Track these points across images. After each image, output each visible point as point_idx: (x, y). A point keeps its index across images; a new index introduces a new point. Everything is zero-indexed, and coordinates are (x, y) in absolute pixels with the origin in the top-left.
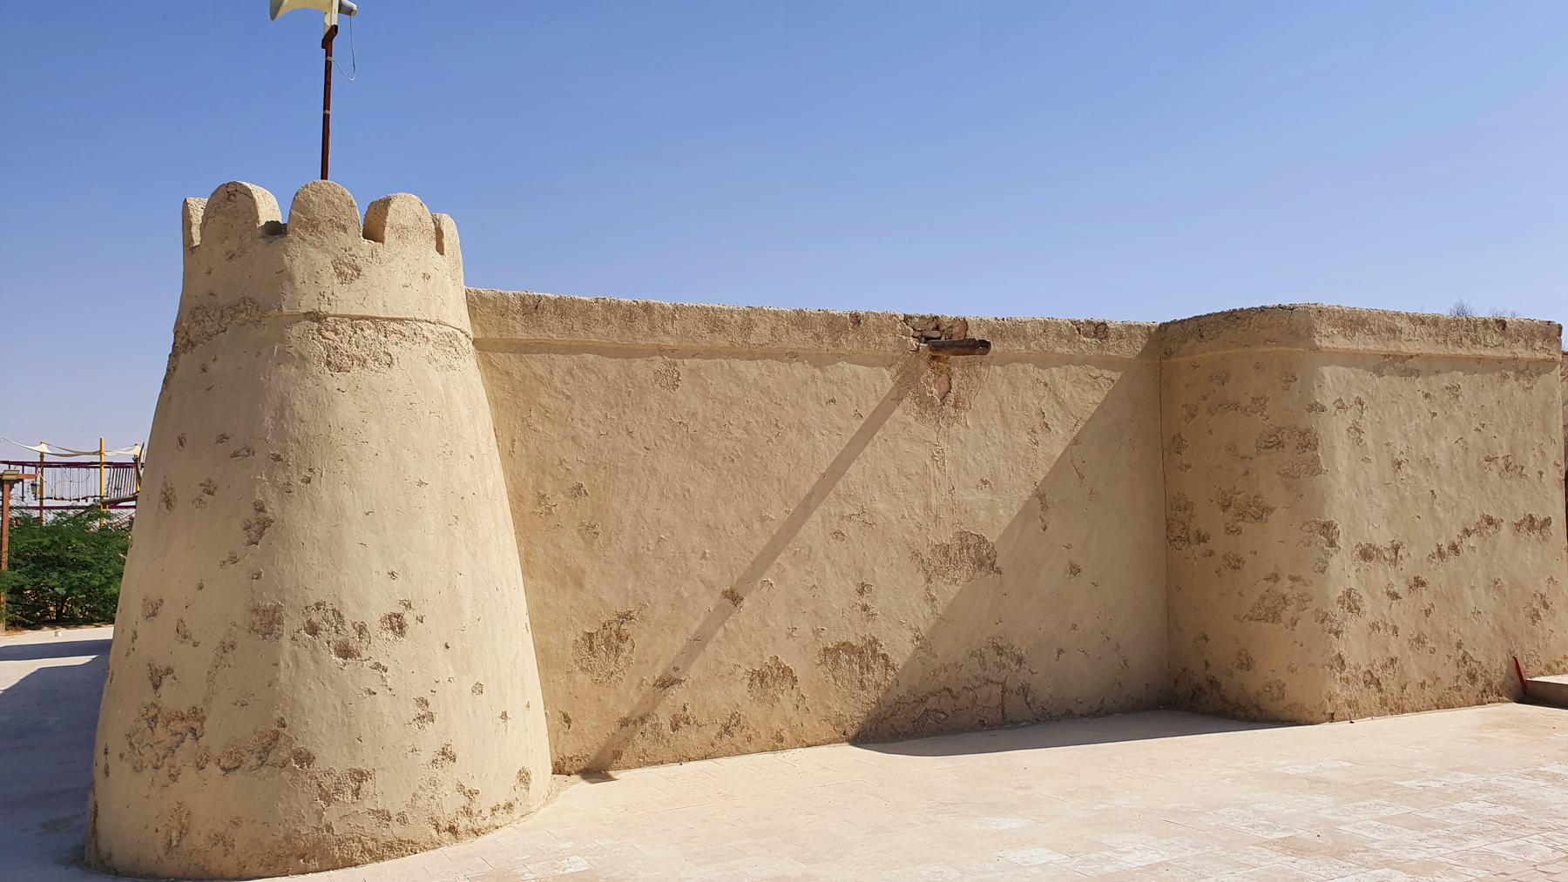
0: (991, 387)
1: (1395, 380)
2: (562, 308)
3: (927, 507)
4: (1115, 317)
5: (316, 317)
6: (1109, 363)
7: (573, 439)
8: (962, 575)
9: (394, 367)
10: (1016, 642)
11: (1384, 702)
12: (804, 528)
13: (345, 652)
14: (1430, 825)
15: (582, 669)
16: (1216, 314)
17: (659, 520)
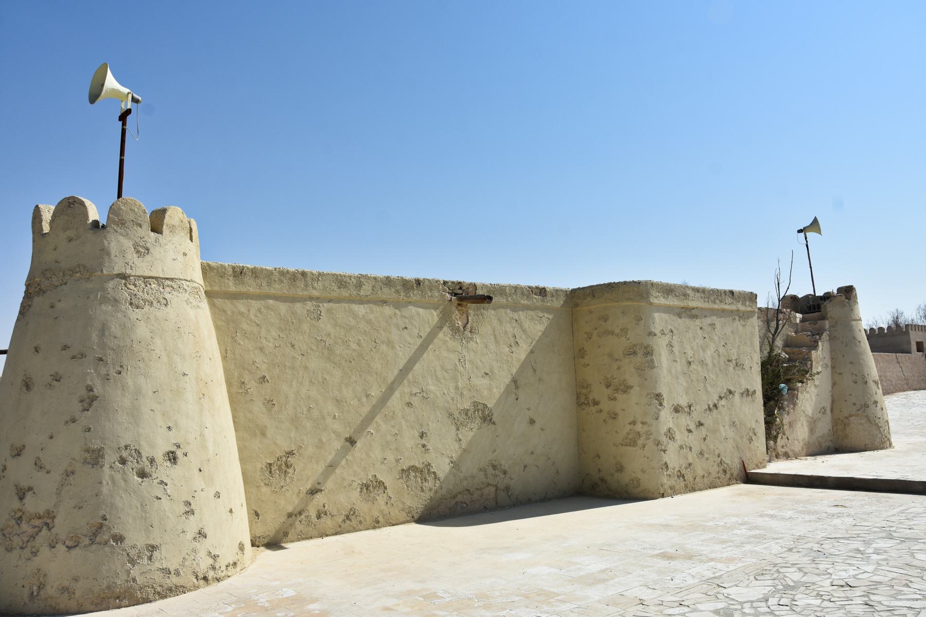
0: (489, 321)
1: (687, 320)
2: (256, 273)
3: (457, 388)
4: (550, 284)
5: (124, 277)
7: (261, 349)
8: (475, 426)
9: (169, 306)
10: (503, 462)
11: (686, 486)
12: (390, 401)
13: (142, 474)
14: (723, 542)
15: (266, 484)
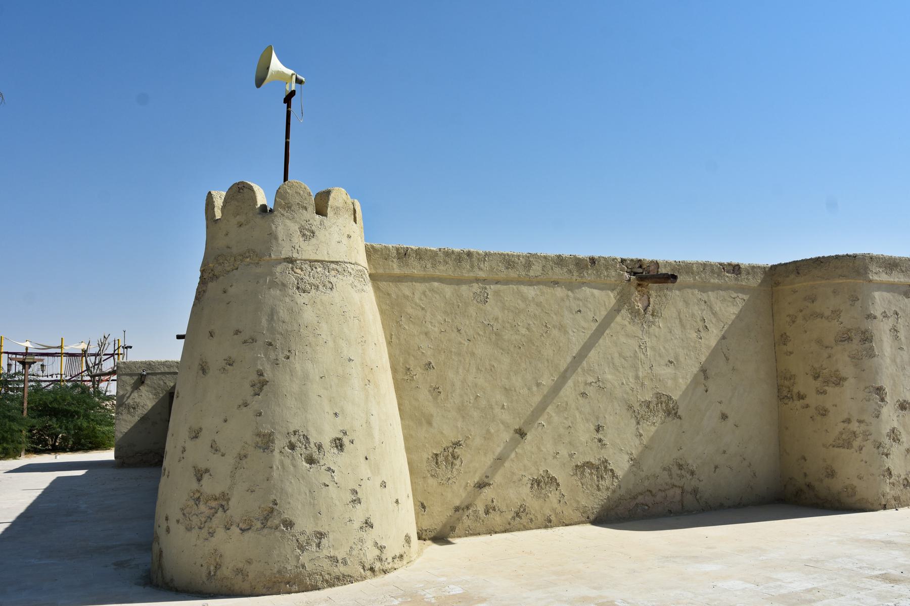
0: (673, 302)
4: (745, 259)
5: (291, 261)
6: (742, 289)
7: (426, 334)
9: (334, 290)
10: (690, 462)
13: (311, 461)
15: (432, 476)
16: (806, 260)
17: (476, 385)
